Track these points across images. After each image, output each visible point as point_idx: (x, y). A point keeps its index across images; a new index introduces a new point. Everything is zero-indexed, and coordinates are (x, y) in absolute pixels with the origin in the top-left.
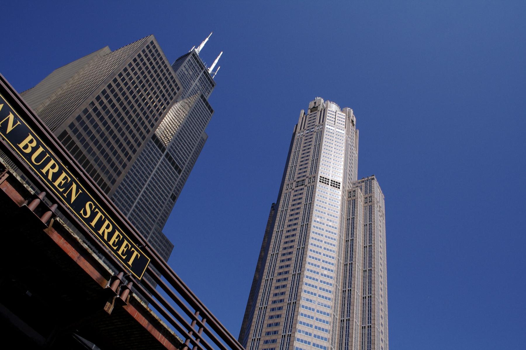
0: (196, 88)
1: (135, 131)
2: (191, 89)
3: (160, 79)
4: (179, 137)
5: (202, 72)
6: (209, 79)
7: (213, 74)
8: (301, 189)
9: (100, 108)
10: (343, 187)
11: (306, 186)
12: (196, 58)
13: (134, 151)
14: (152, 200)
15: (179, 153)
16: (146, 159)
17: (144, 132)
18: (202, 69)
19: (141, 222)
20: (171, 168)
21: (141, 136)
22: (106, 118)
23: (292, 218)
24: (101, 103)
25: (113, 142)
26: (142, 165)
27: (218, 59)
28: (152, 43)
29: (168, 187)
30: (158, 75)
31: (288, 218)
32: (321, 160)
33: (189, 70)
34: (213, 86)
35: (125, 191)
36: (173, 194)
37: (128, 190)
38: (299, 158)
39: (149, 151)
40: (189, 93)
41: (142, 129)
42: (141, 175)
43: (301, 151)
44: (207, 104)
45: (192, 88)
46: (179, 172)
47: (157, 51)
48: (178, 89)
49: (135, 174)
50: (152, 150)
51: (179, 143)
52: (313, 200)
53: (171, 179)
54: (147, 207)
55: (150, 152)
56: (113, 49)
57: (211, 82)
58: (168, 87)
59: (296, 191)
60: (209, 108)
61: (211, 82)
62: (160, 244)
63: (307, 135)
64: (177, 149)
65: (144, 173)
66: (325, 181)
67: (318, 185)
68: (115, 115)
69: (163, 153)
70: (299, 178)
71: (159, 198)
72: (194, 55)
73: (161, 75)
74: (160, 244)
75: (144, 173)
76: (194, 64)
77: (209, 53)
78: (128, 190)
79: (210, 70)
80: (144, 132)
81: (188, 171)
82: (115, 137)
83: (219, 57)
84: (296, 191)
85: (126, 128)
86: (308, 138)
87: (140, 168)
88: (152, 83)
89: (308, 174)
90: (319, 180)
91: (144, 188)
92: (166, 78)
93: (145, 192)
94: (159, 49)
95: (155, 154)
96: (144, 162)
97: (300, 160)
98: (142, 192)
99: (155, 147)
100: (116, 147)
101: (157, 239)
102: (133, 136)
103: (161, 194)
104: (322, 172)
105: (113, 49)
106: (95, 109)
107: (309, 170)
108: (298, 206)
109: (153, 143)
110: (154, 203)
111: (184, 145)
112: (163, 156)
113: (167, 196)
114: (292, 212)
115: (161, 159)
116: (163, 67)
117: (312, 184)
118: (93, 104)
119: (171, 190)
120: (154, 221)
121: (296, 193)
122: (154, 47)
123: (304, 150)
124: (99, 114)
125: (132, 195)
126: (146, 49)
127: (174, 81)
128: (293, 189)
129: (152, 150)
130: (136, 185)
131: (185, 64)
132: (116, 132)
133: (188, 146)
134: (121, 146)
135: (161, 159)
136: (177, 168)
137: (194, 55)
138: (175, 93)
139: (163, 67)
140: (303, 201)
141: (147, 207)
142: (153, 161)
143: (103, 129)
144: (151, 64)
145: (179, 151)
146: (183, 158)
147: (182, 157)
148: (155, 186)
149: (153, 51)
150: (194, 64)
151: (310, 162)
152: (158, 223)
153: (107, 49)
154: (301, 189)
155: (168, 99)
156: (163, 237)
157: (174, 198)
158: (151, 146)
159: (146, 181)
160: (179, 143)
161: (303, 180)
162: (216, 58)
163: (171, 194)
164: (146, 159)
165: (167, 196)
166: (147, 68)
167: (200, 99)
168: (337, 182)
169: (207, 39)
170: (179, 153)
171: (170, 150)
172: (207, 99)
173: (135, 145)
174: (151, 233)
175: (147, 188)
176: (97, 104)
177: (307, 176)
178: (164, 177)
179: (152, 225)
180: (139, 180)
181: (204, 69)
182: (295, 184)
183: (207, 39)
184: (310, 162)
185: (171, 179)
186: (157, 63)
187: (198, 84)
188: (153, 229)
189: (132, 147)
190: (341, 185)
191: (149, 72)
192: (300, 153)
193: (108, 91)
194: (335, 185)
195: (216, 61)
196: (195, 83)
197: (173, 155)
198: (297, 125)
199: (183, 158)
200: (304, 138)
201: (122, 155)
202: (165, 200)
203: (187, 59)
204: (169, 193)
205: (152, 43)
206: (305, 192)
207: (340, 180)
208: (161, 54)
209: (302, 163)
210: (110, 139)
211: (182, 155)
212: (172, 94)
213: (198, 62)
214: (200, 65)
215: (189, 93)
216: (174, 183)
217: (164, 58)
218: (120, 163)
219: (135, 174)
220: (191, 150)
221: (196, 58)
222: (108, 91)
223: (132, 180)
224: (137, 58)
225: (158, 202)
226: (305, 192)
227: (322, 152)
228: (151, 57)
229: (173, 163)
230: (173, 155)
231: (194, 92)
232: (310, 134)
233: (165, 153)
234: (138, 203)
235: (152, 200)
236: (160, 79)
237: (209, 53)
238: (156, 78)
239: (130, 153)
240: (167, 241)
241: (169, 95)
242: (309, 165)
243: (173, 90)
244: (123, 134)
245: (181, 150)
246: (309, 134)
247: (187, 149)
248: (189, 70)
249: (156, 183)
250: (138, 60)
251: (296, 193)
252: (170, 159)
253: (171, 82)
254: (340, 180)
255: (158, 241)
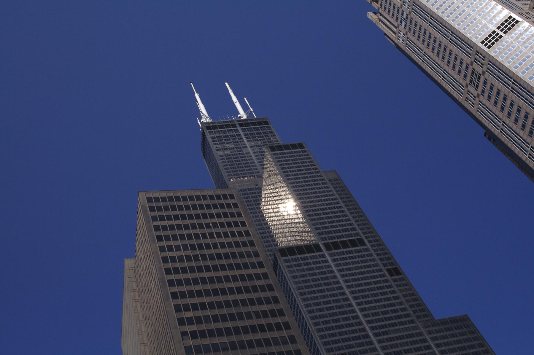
0: (257, 150)
1: (254, 296)
2: (254, 158)
3: (205, 216)
4: (312, 215)
5: (239, 128)
6: (254, 124)
7: (250, 115)
8: (485, 83)
9: (194, 328)
10: (520, 14)
11: (483, 73)
12: (215, 127)
13: (281, 313)
14: (379, 307)
15: (334, 227)
16: (315, 280)
17: (262, 282)
18: (234, 126)
19: (401, 341)
20: (350, 252)
21: (265, 291)
22: (213, 326)
23: (520, 123)
24: (190, 321)
25: (251, 337)
26: (321, 291)
27: (232, 94)
28: (149, 200)
29: (373, 271)
30: (198, 216)
31: (517, 128)
32: (457, 27)
33: (226, 145)
34: (266, 123)
35: (344, 337)
36: (387, 270)
37: (346, 333)
38: (437, 59)
39: (308, 270)
40: (257, 164)
41: (257, 283)
42: (334, 301)
43: (427, 51)
44: (287, 147)
45: (253, 155)
46: (362, 243)
47: (164, 199)
48: (232, 197)
49: (328, 309)
50: (307, 264)
51: (320, 219)
52: (511, 75)
53: (365, 261)
54: (387, 319)
55: (310, 269)
56: (132, 254)
57: (260, 123)
58: (220, 211)
59: (483, 92)
60: (294, 146)
61: (260, 123)
62: (451, 332)
63: (407, 28)
64: (328, 227)
65: (334, 295)
66: (493, 39)
67: (493, 54)
68: (217, 312)
69: (321, 251)
70: (465, 76)
71: (382, 294)
72: (208, 126)
73: (199, 212)
74: (451, 332)
75: (334, 295)
76: (222, 135)
77: (218, 104)
78: (346, 333)
79: (242, 114)
80: (262, 282)
81: (369, 228)
82: (245, 330)
83: (230, 91)
84: (483, 92)
85: (243, 305)
86: (414, 29)
87: (324, 297)
88: (202, 231)
89: (467, 60)
90: (485, 49)
91: (356, 308)
92: (208, 207)
93: (362, 310)
94: (164, 195)
95: (316, 263)
96: (318, 285)
97: (439, 60)
98: (360, 314)
99: (307, 258)
100: (259, 336)
101: (442, 334)
102: (260, 302)
103: (378, 288)
104: (476, 36)
105: (132, 254)
106: (194, 335)
107: (461, 55)
108: (508, 102)
109: (299, 256)
110: (384, 306)
111: (326, 213)
112: (326, 253)
113: (387, 281)
114: (513, 117)
115: (328, 258)
116: (190, 203)
117: (486, 62)
118: (184, 334)
119: (380, 270)
120: (412, 322)
121: (486, 94)
122: (157, 199)
123: (428, 45)
124: (203, 334)
125: (355, 331)
126: (153, 214)
127: (218, 197)
128: (478, 95)
129: (307, 264)
130: (345, 316)
131: (214, 148)
132: (239, 324)
133: (332, 208)
134: (262, 328)
135: (328, 258)
136: (353, 243)
137: (208, 128)
138: (236, 205)
139: (190, 203)
140: (505, 90)
141: (387, 319)
142: (325, 273)
143: (225, 339)
144: (176, 217)
145: (332, 227)
146: (345, 225)
147: (342, 225)
148: (362, 291)
149: (161, 204)
150: (222, 135)
151: (451, 46)
152: (418, 317)
153: (129, 263)
154: (485, 83)
155: (237, 219)
156: (444, 322)
157: (395, 271)
158: (301, 262)
159: (347, 299)
160: (320, 219)
161: (473, 73)
162: (230, 97)
163: (386, 273)
164: (315, 280)
165: (387, 281)
166: (179, 227)
167: (275, 154)
168: (506, 21)
169: (197, 95)
170: (334, 227)
171: (323, 239)
172: (281, 143)
173: (273, 306)
174: (427, 337)
175: (359, 304)
176: (188, 328)
177: (469, 62)
178: (356, 268)
179: (416, 328)
180: (340, 307)
181: (237, 123)
182: (471, 89)
183: (197, 95)
184: (451, 46)
185: (365, 261)
186: (180, 208)
187: (253, 144)
188: (423, 330)
189: (273, 314)
190: (514, 16)
191: (186, 227)
192: (430, 54)
193: (180, 302)
194: (508, 25)
195: (234, 99)
196: (249, 147)
197: (332, 238)
198: (386, 35)
199: (345, 225)
200: (410, 35)
201: (276, 334)
202: (390, 286)
203: (210, 140)
204: (383, 276)
205: (149, 200)
206: (492, 80)
207: (505, 13)
208: (171, 194)
209: (446, 60)
210: (245, 337)
211: (340, 226)
212: (233, 210)
213: (221, 127)
214: (227, 126)
215: (257, 164)
216: (374, 260)
217: (179, 194)
218: (285, 343)
219: (328, 309)
220: (340, 207)
221: (215, 127)
222: (180, 302)
223: (335, 318)
224: (158, 233)
225: (388, 299)
226: (492, 80)
227: (446, 19)
228: (167, 213)
229: (345, 244)
230: (332, 238)
231: (261, 157)
232: (408, 23)
233: (323, 248)
234: (372, 328)
235: (379, 307)
236: (205, 216)
237: (218, 104)
238: (199, 221)
239: (279, 320)
240: (453, 320)
241: (232, 215)
242: (455, 50)
243: (229, 206)
244: (249, 316)
245: (331, 222)
246: (408, 24)
247: (334, 212)
248: (226, 145)
249: (358, 285)
250: (162, 233)
251: (486, 94)
252: (336, 246)
253: (216, 202)
254: (505, 13)
255: (446, 333)
